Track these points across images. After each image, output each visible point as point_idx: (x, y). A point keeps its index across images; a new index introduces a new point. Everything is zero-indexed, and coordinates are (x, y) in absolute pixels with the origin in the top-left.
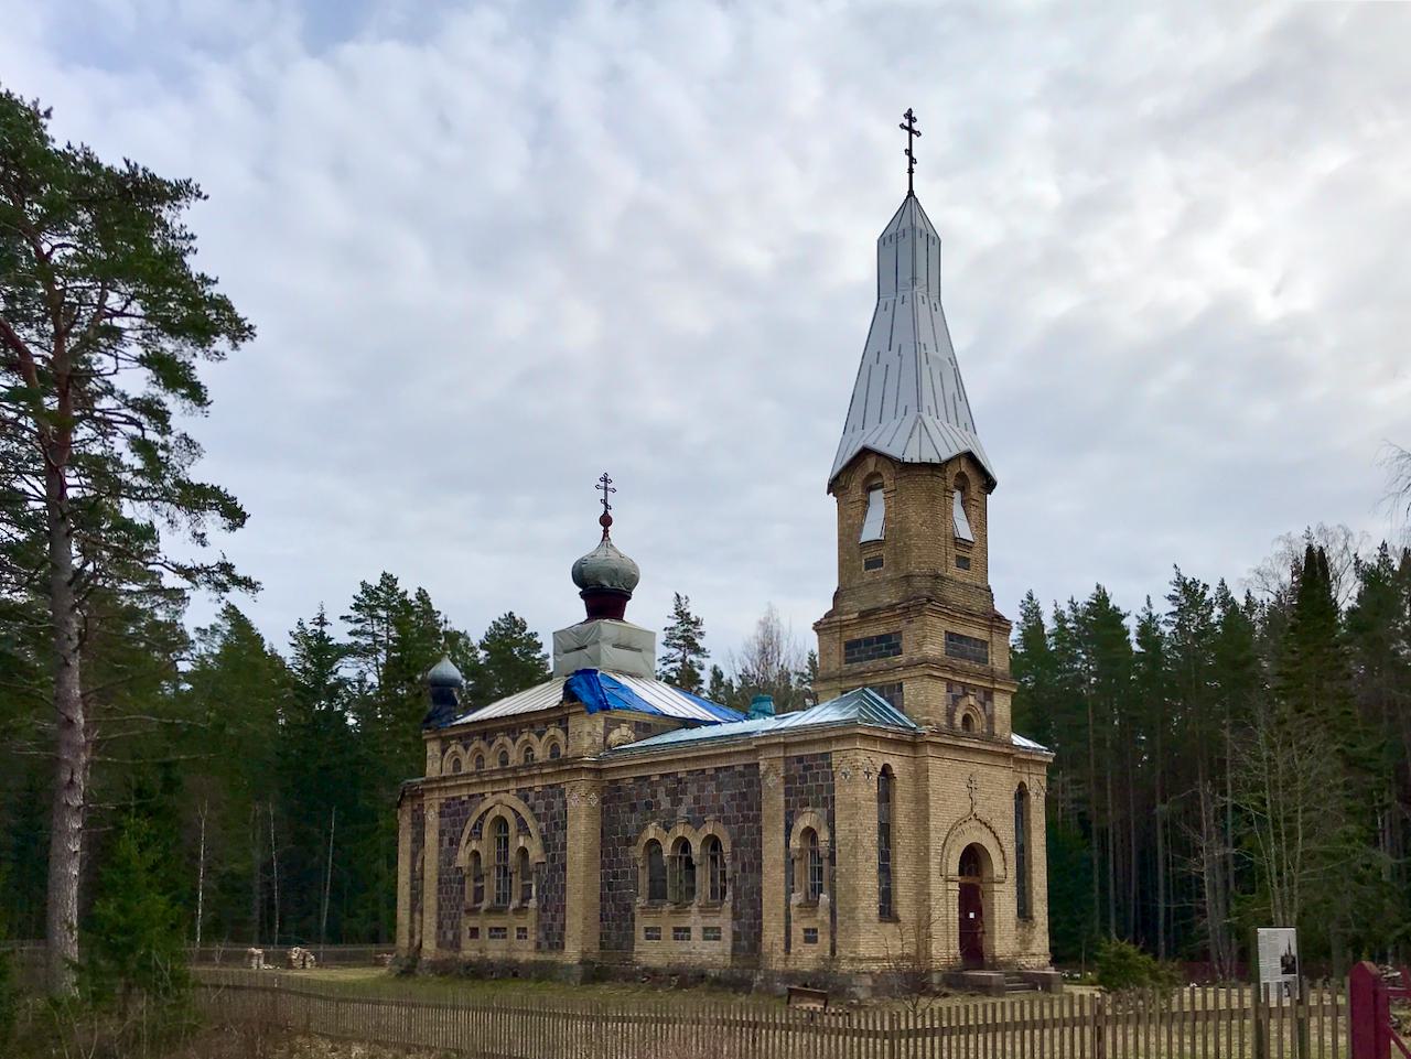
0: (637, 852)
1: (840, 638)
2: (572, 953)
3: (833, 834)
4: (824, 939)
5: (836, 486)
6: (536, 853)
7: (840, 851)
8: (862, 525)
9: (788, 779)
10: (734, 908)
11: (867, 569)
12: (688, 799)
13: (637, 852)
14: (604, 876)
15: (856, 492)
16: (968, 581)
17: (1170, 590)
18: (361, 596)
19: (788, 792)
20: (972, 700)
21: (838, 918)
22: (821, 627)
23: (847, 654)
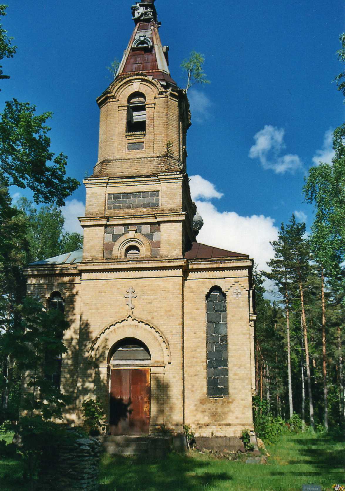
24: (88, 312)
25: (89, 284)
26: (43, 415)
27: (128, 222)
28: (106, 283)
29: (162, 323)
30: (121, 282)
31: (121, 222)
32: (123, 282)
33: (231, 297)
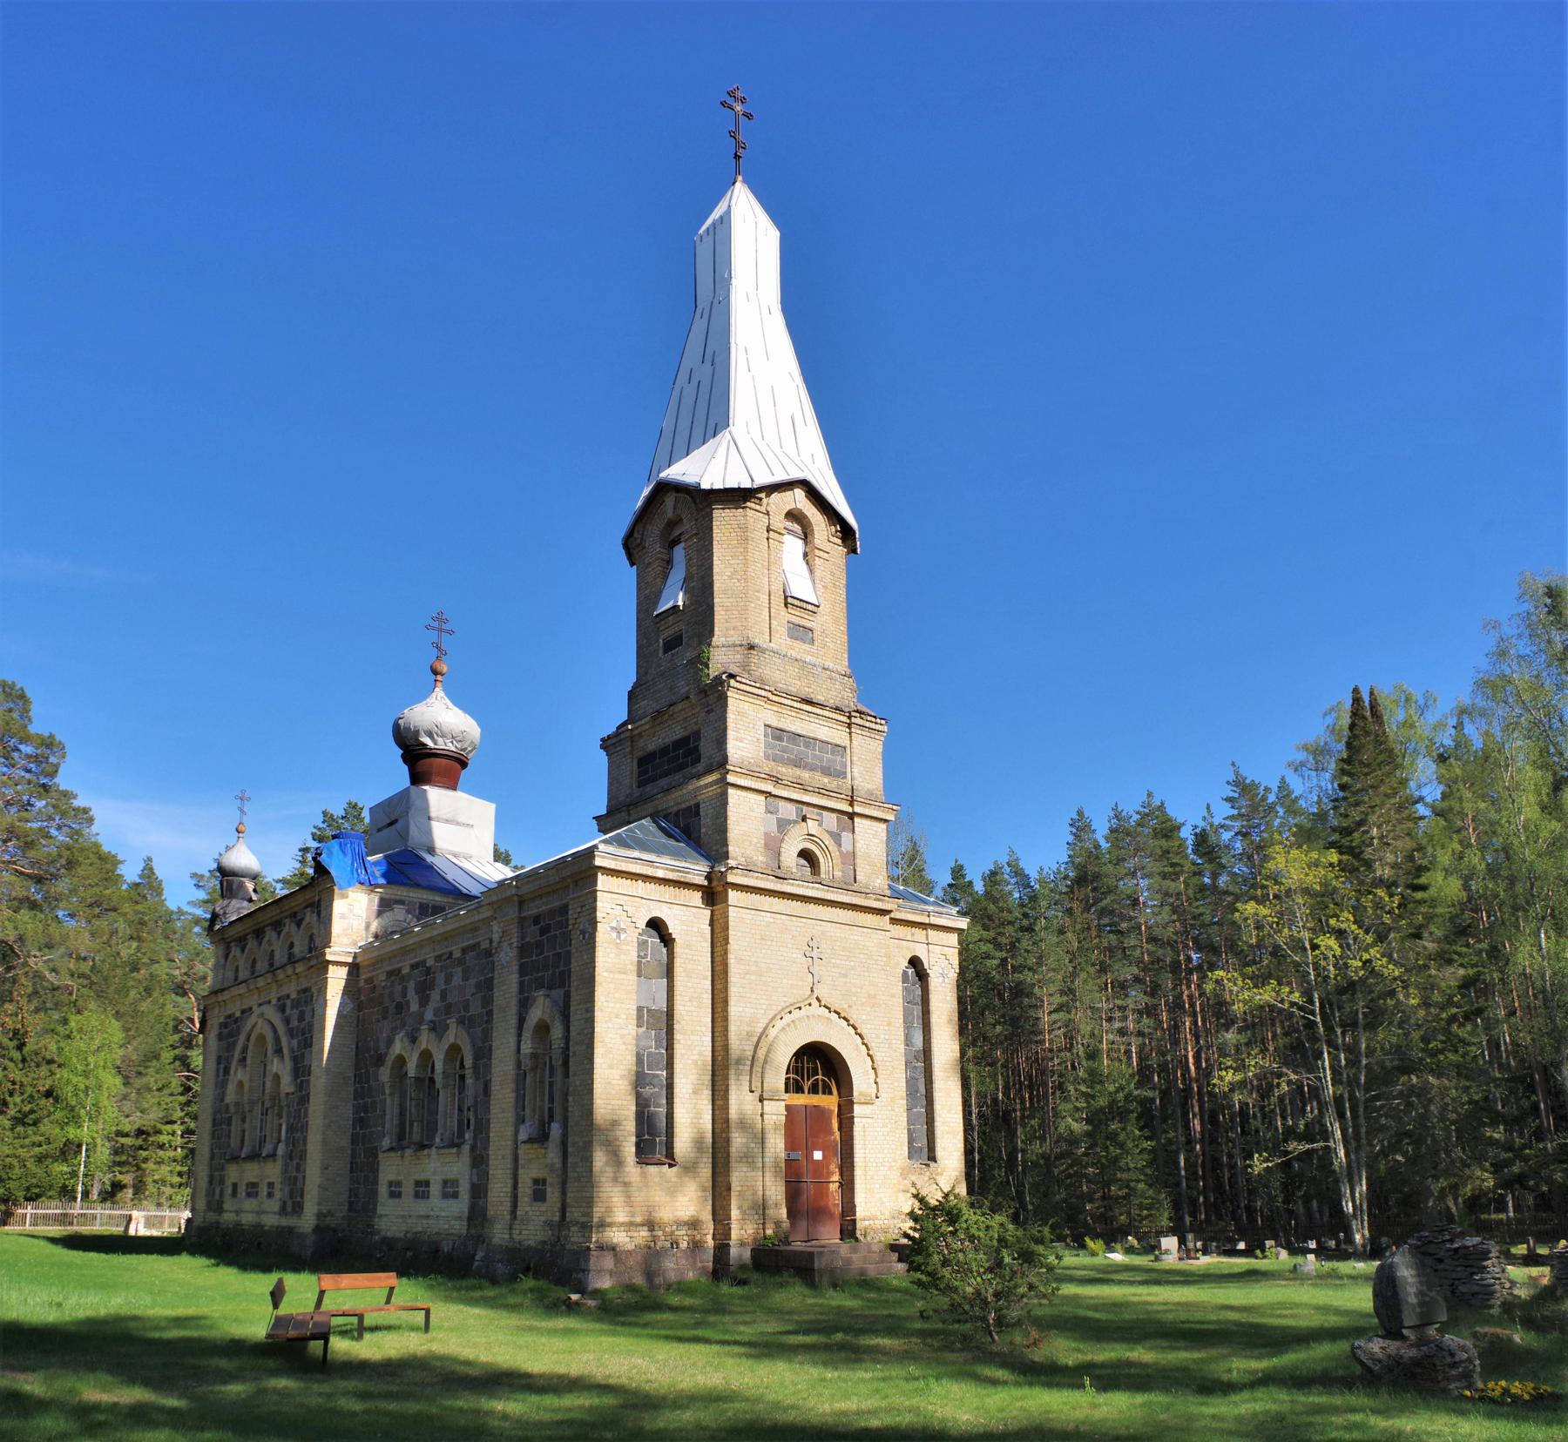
0: (385, 1074)
1: (631, 752)
2: (307, 1221)
3: (567, 1029)
4: (553, 1194)
5: (632, 545)
6: (287, 1085)
7: (574, 1053)
8: (661, 592)
9: (523, 950)
10: (473, 1148)
11: (665, 651)
12: (435, 996)
13: (385, 1074)
14: (357, 1109)
15: (654, 547)
16: (808, 659)
17: (1229, 791)
18: (322, 825)
19: (523, 970)
20: (812, 826)
21: (570, 1160)
22: (610, 742)
23: (640, 774)
24: (744, 978)
25: (744, 916)
26: (1519, 1317)
27: (806, 798)
28: (772, 920)
29: (864, 1017)
30: (796, 924)
31: (795, 796)
32: (800, 924)
33: (936, 980)
